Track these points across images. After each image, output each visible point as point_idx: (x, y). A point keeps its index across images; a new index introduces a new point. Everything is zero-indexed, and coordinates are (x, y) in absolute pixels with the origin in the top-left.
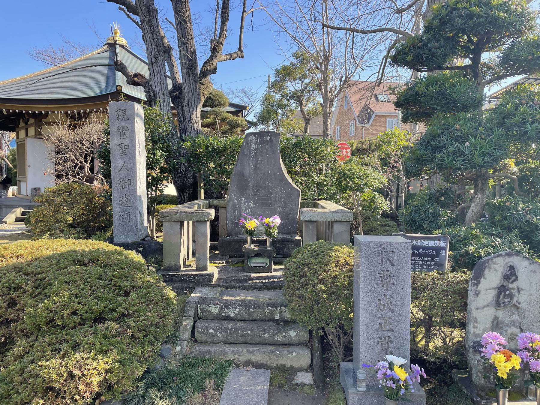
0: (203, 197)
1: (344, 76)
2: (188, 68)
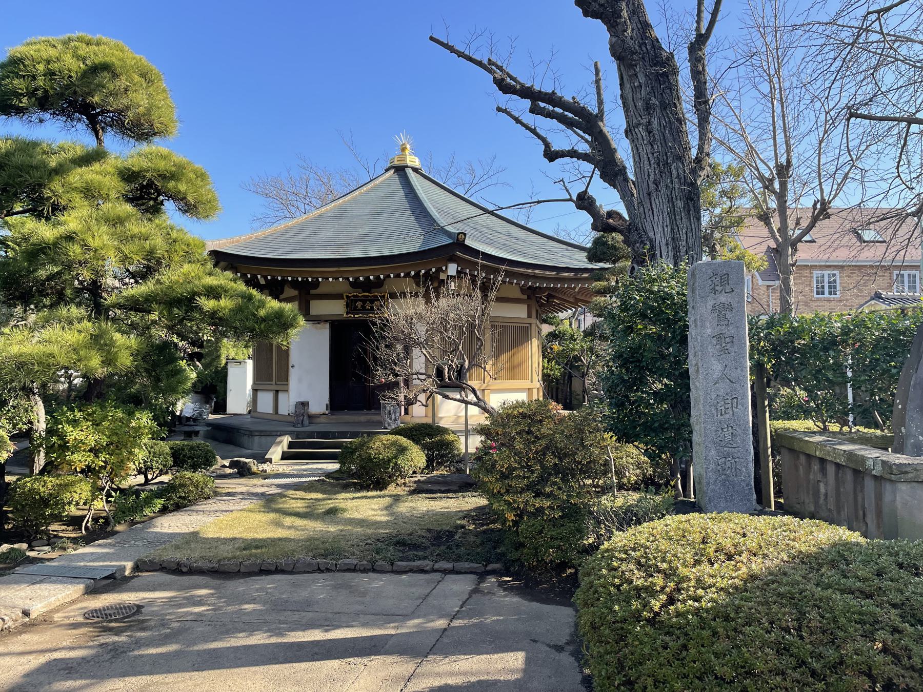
2: (687, 199)
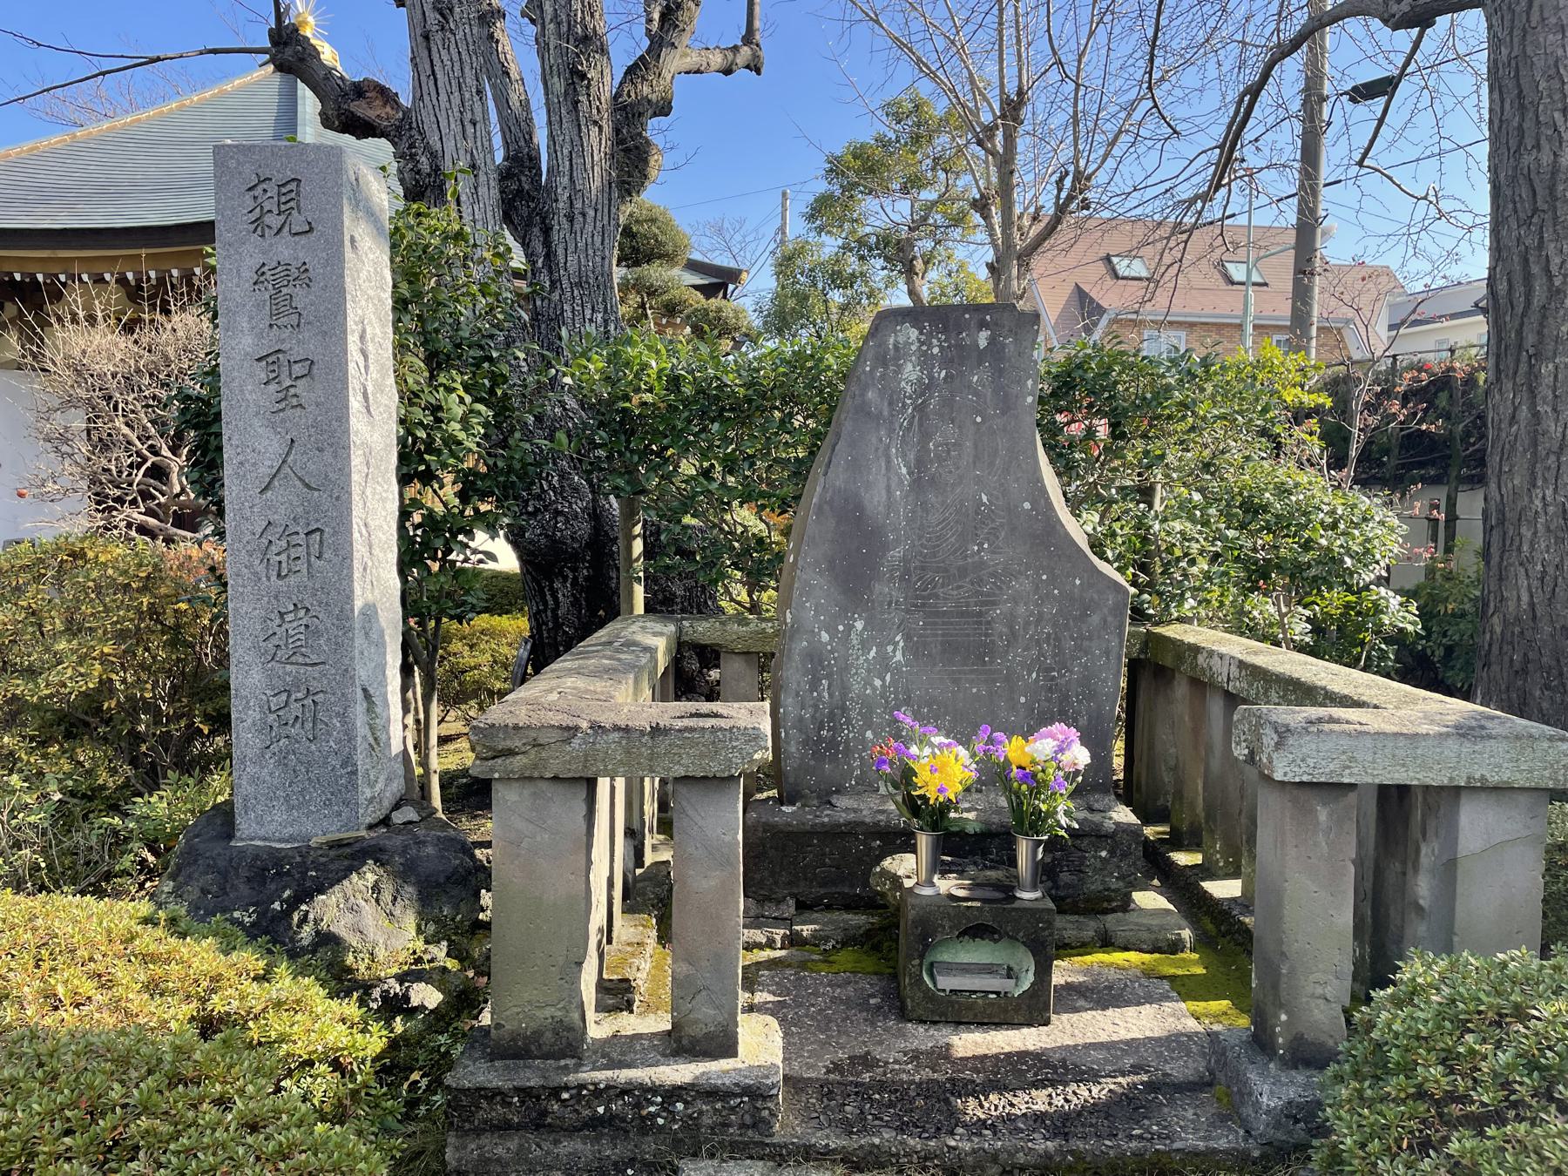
0: (639, 608)
1: (1071, 168)
